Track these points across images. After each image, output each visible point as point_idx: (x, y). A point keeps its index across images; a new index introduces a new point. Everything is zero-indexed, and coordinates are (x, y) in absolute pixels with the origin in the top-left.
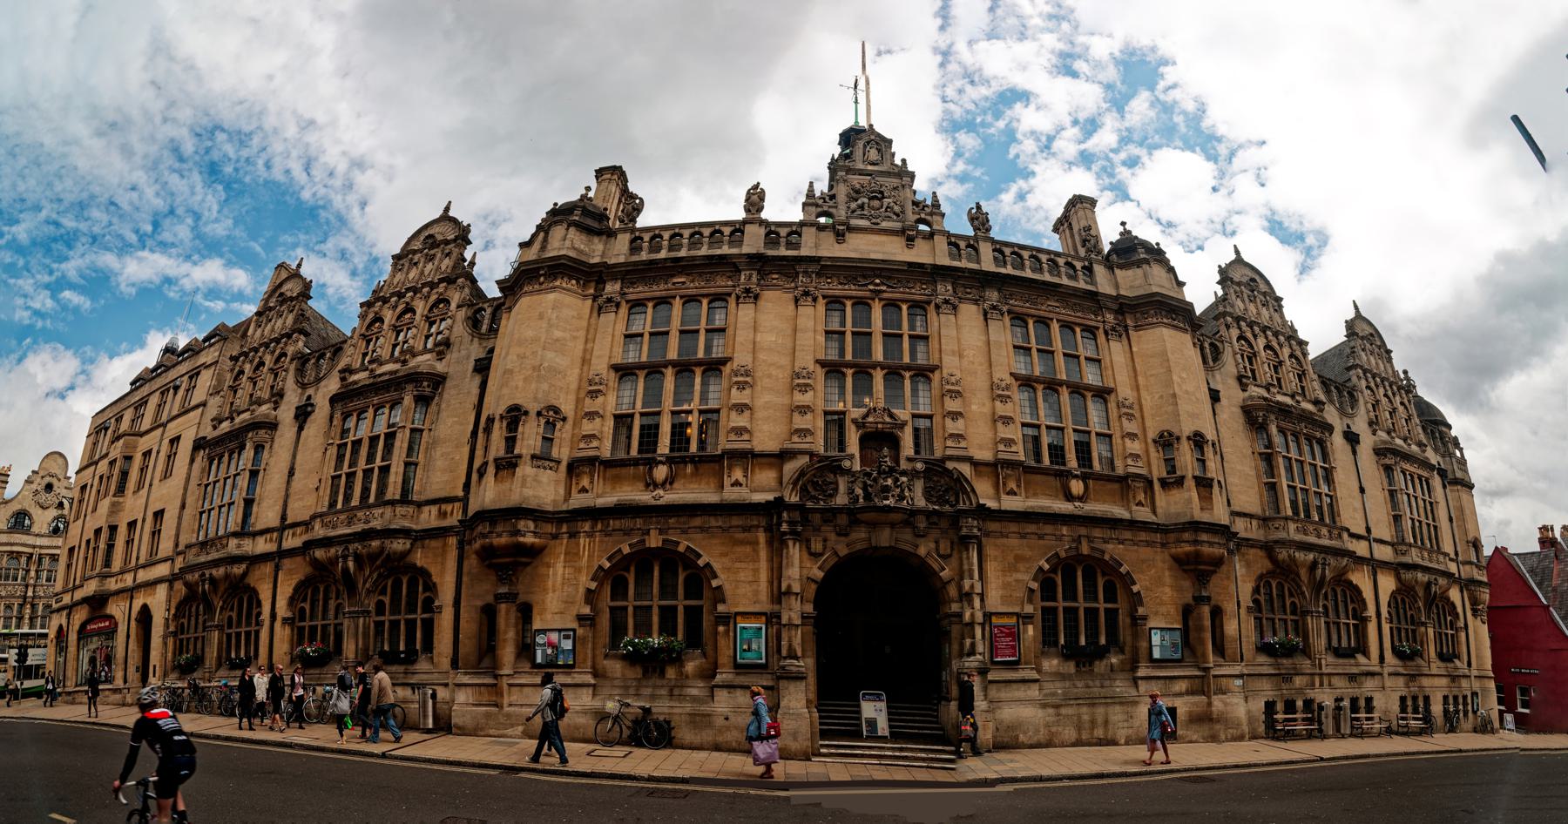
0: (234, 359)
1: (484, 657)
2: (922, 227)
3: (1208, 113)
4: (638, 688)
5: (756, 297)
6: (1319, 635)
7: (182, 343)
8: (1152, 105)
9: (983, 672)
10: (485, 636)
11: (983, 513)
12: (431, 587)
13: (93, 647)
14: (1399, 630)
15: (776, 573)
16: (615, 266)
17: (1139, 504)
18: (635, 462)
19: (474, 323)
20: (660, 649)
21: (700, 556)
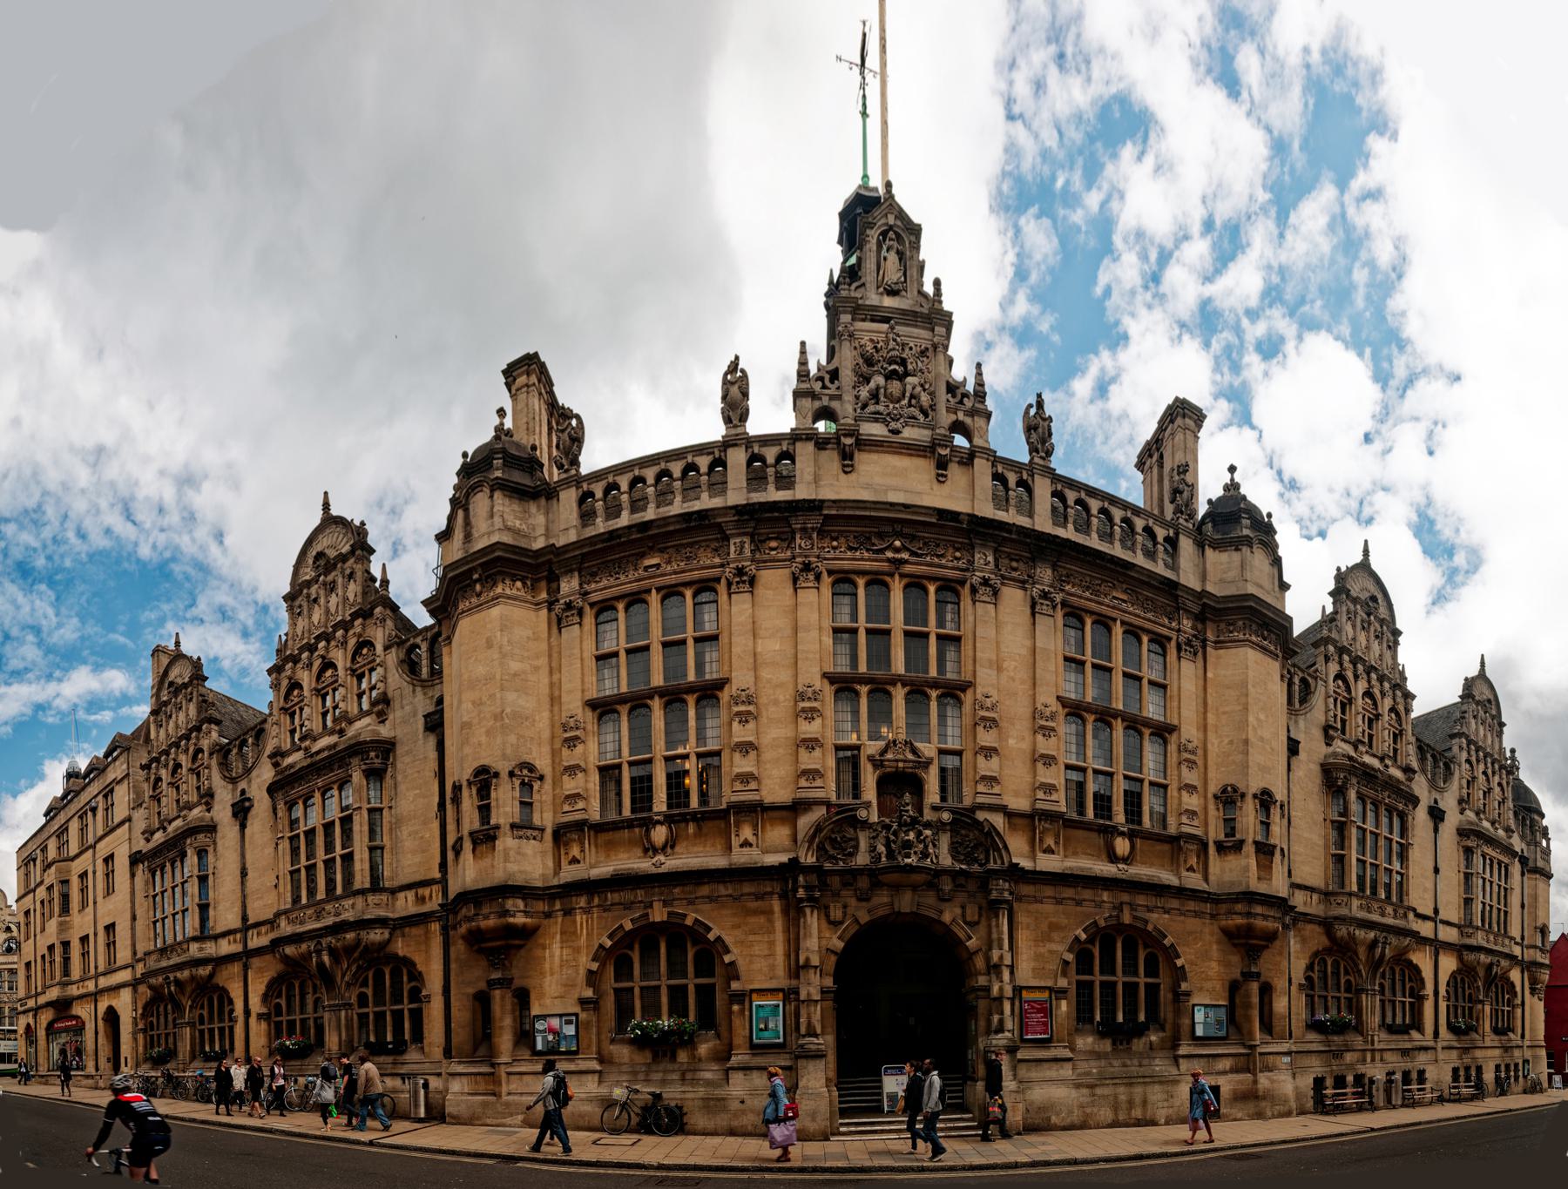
2: (960, 441)
3: (1407, 283)
4: (647, 1073)
5: (752, 582)
6: (1373, 1013)
7: (83, 764)
8: (1331, 227)
9: (1012, 1050)
10: (479, 1024)
12: (416, 976)
13: (62, 1041)
14: (1456, 1008)
15: (794, 945)
17: (1191, 869)
18: (629, 824)
19: (411, 666)
20: (670, 1032)
21: (709, 929)
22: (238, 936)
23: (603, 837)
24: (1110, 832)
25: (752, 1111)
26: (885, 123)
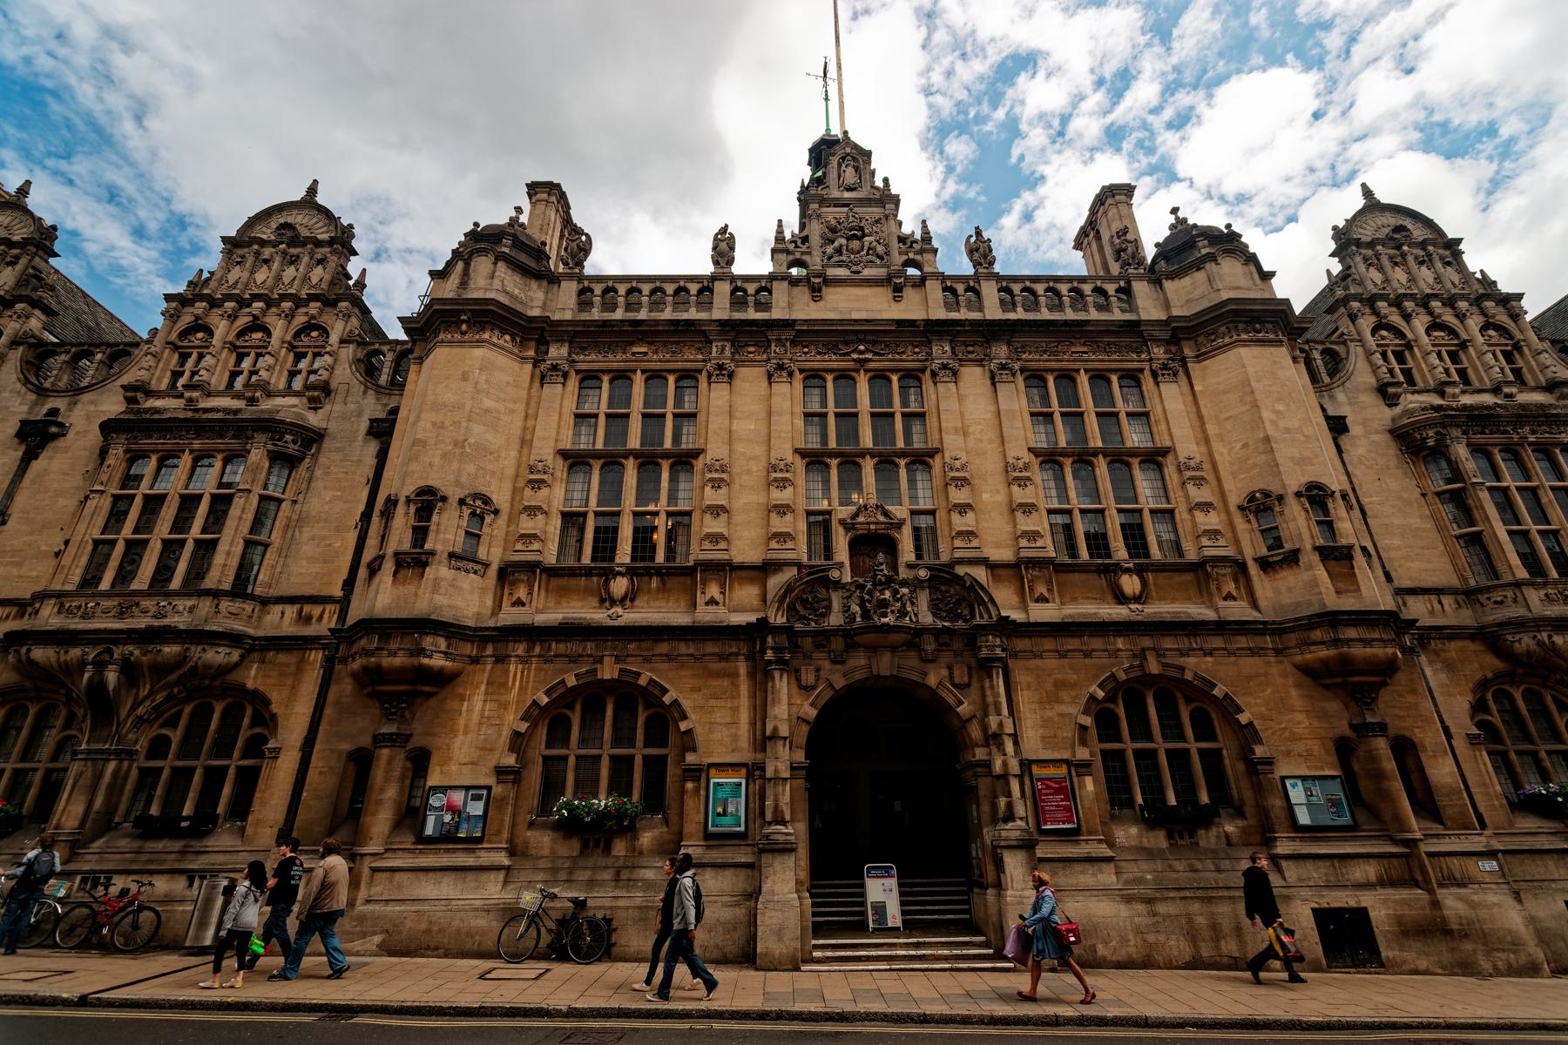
2: (912, 271)
4: (571, 871)
5: (731, 375)
9: (1027, 845)
10: (347, 794)
11: (1007, 628)
12: (267, 720)
15: (760, 711)
16: (560, 323)
17: (1229, 597)
18: (588, 572)
19: (369, 369)
21: (665, 691)
23: (555, 582)
24: (1112, 571)
26: (841, 103)
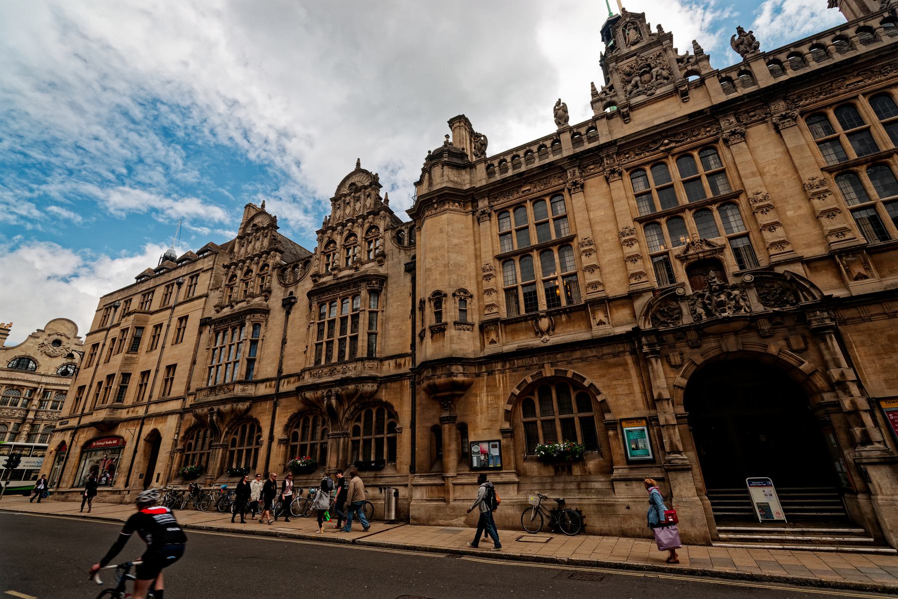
0: (228, 267)
1: (434, 463)
2: (692, 78)
5: (582, 186)
7: (179, 254)
10: (434, 448)
11: (829, 303)
12: (394, 415)
13: (96, 458)
15: (647, 385)
16: (481, 188)
18: (525, 319)
19: (398, 240)
20: (565, 453)
21: (584, 379)
22: (273, 383)
23: (509, 327)
25: (637, 516)
